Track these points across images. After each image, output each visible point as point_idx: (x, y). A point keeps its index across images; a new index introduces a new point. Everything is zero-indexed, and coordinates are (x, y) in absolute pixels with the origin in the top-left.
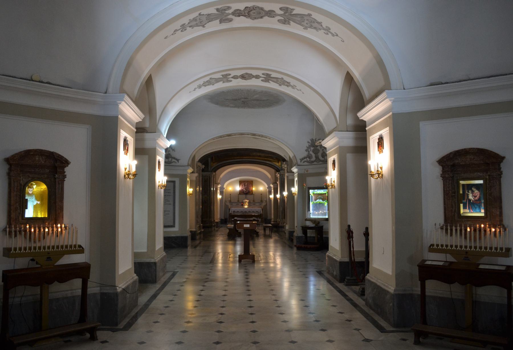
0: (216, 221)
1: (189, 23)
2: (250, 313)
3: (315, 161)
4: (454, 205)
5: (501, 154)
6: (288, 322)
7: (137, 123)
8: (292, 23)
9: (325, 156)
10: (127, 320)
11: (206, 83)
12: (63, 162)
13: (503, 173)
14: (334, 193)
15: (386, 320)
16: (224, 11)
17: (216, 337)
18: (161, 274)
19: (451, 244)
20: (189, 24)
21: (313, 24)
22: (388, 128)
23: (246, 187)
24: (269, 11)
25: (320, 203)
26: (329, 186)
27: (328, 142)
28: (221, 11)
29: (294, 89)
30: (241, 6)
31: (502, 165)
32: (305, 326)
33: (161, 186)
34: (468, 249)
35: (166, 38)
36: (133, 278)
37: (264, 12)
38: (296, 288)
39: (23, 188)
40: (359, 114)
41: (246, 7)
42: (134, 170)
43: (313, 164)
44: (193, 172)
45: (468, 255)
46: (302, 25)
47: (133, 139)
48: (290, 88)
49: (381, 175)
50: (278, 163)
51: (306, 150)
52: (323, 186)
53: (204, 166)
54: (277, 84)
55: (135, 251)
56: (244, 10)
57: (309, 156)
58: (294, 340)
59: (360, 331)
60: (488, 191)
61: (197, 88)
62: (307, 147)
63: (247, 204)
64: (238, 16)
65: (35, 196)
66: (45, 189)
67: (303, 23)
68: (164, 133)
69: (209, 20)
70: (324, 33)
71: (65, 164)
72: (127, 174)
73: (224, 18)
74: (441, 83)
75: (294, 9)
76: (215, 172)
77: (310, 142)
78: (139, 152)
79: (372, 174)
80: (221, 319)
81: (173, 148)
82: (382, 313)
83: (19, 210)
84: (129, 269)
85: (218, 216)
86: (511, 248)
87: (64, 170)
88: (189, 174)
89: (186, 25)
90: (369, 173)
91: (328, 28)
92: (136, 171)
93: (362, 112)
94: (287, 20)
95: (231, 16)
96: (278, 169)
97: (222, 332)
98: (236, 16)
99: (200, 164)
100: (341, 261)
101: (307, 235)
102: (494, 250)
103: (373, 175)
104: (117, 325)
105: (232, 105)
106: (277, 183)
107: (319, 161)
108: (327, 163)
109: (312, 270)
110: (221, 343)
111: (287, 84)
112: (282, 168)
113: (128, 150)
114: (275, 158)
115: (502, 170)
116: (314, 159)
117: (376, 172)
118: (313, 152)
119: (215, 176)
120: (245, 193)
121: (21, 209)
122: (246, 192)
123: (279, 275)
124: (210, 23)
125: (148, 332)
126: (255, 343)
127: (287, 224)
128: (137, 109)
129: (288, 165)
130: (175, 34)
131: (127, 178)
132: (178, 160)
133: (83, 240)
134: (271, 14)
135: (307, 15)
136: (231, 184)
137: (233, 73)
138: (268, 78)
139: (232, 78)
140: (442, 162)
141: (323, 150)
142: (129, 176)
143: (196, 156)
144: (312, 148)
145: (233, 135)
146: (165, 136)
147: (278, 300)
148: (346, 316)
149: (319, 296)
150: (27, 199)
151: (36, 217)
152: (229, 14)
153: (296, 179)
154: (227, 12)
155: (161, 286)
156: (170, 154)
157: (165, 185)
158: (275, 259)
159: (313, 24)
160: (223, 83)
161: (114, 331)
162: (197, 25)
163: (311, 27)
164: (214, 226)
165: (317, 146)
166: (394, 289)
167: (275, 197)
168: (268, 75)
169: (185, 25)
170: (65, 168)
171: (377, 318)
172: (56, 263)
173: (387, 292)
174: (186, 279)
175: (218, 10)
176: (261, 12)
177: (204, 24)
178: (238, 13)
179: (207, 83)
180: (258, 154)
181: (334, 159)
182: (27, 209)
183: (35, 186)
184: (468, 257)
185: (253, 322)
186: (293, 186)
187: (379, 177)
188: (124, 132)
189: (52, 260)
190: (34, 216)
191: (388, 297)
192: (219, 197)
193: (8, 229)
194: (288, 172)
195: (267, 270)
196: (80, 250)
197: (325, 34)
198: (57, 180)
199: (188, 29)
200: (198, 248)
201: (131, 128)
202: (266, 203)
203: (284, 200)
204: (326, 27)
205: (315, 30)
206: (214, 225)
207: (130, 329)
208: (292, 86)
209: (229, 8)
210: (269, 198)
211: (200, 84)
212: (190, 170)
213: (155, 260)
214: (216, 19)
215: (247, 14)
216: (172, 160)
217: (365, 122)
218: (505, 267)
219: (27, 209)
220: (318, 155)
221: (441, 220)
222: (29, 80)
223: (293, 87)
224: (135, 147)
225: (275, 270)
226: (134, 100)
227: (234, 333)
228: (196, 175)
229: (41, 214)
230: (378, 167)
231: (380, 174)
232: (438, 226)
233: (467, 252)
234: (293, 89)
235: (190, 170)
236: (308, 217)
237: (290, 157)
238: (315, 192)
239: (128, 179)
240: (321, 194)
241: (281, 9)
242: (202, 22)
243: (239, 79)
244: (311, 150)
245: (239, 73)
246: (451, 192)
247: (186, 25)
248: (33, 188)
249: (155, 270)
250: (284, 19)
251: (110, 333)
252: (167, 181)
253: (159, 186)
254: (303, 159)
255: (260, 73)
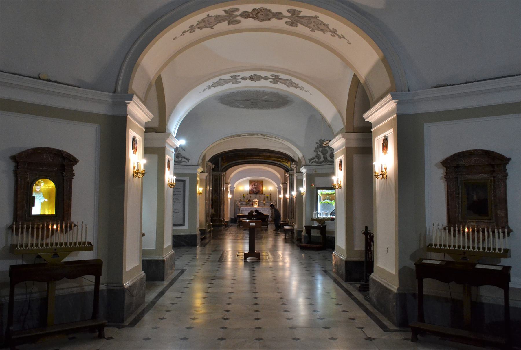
0: (226, 220)
1: (197, 24)
2: (255, 310)
3: (323, 162)
4: (458, 206)
5: (507, 155)
6: (292, 319)
7: (146, 123)
8: (299, 25)
9: (332, 156)
10: (133, 316)
11: (215, 83)
12: (72, 160)
13: (509, 174)
14: (340, 193)
15: (390, 319)
16: (232, 13)
17: (221, 333)
18: (170, 271)
19: (449, 244)
20: (197, 26)
21: (320, 26)
22: (392, 130)
23: (256, 186)
24: (276, 13)
25: (328, 203)
26: (336, 186)
27: (335, 143)
28: (229, 12)
29: (302, 90)
30: (249, 8)
31: (507, 167)
32: (312, 325)
33: (171, 185)
34: (466, 249)
35: (174, 39)
36: (140, 275)
37: (271, 14)
38: (304, 287)
39: (31, 185)
40: (365, 116)
41: (254, 9)
42: (142, 169)
43: (321, 164)
44: (203, 172)
45: (467, 255)
46: (309, 27)
47: (142, 138)
48: (298, 89)
49: (385, 176)
50: (288, 163)
51: (315, 151)
52: (330, 186)
53: (214, 166)
54: (286, 86)
55: (143, 249)
56: (252, 12)
57: (318, 157)
58: (297, 337)
59: (362, 329)
60: (492, 192)
61: (207, 89)
62: (315, 147)
63: (256, 204)
64: (246, 18)
65: (43, 193)
66: (52, 186)
67: (310, 25)
68: (173, 133)
69: (217, 22)
70: (331, 35)
71: (73, 162)
72: (136, 173)
73: (232, 20)
74: (447, 85)
75: (301, 11)
76: (225, 171)
77: (319, 142)
78: (147, 151)
79: (376, 174)
80: (226, 316)
81: (183, 148)
82: (385, 313)
83: (26, 207)
84: (137, 267)
85: (228, 214)
86: (510, 249)
87: (72, 168)
88: (199, 173)
89: (194, 26)
90: (374, 174)
91: (334, 30)
92: (144, 170)
93: (368, 114)
94: (295, 22)
95: (239, 18)
96: (288, 170)
97: (227, 328)
98: (244, 18)
99: (210, 164)
100: (346, 260)
101: (310, 234)
102: (487, 250)
103: (378, 175)
104: (123, 321)
105: (241, 106)
106: (286, 183)
107: (328, 162)
108: (334, 164)
109: (318, 268)
110: (225, 339)
111: (296, 86)
112: (291, 168)
113: (136, 149)
114: (284, 158)
115: (507, 171)
116: (322, 159)
117: (380, 173)
118: (321, 153)
119: (225, 176)
120: (255, 192)
121: (28, 207)
122: (256, 191)
123: (287, 273)
124: (218, 24)
125: (153, 328)
126: (259, 339)
127: (295, 223)
128: (147, 109)
129: (297, 166)
130: (184, 35)
131: (136, 177)
132: (188, 160)
133: (90, 238)
134: (278, 16)
135: (314, 17)
136: (241, 184)
137: (242, 74)
138: (276, 80)
139: (241, 79)
140: (446, 163)
141: (331, 151)
142: (138, 174)
143: (206, 155)
144: (321, 149)
145: (243, 135)
146: (175, 136)
147: (283, 298)
148: (351, 315)
149: (326, 294)
150: (34, 197)
151: (44, 214)
152: (237, 16)
153: (305, 179)
154: (235, 14)
155: (169, 283)
156: (180, 154)
157: (174, 184)
158: (284, 258)
159: (320, 26)
160: (232, 84)
161: (119, 327)
162: (206, 27)
163: (318, 29)
164: (224, 225)
165: (325, 147)
166: (397, 288)
167: (284, 198)
168: (276, 77)
169: (194, 26)
170: (73, 166)
171: (380, 317)
172: (62, 260)
173: (390, 291)
174: (194, 277)
175: (226, 11)
176: (269, 14)
177: (212, 25)
178: (246, 15)
179: (216, 84)
180: (268, 154)
181: (341, 159)
182: (34, 206)
183: (42, 184)
184: (466, 257)
185: (257, 319)
186: (302, 185)
187: (383, 178)
188: (133, 131)
189: (58, 257)
190: (42, 214)
191: (391, 296)
192: (229, 196)
193: (15, 226)
194: (297, 172)
195: (276, 268)
196: (89, 247)
197: (332, 37)
198: (65, 178)
199: (197, 30)
200: (207, 246)
201: (141, 128)
202: (276, 202)
203: (293, 200)
204: (333, 29)
205: (322, 32)
206: (223, 224)
207: (136, 326)
208: (300, 88)
209: (237, 10)
210: (279, 198)
211: (209, 85)
212: (200, 170)
213: (163, 258)
214: (224, 20)
215: (254, 16)
216: (182, 159)
217: (371, 123)
218: (502, 267)
219: (34, 206)
220: (326, 156)
221: (444, 221)
222: (36, 78)
223: (301, 88)
224: (144, 146)
225: (283, 269)
226: (143, 100)
227: (239, 329)
228: (206, 174)
229: (49, 212)
230: (382, 167)
231: (384, 174)
232: (441, 227)
233: (465, 252)
234: (301, 91)
235: (200, 170)
236: (315, 217)
237: (299, 158)
238: (324, 192)
239: (137, 177)
240: (329, 194)
241: (288, 11)
242: (210, 24)
243: (248, 80)
244: (319, 151)
245: (248, 74)
246: (454, 193)
247: (194, 26)
248: (41, 186)
249: (164, 268)
250: (292, 20)
251: (116, 330)
252: (177, 180)
253: (168, 185)
254: (311, 159)
255: (268, 74)
